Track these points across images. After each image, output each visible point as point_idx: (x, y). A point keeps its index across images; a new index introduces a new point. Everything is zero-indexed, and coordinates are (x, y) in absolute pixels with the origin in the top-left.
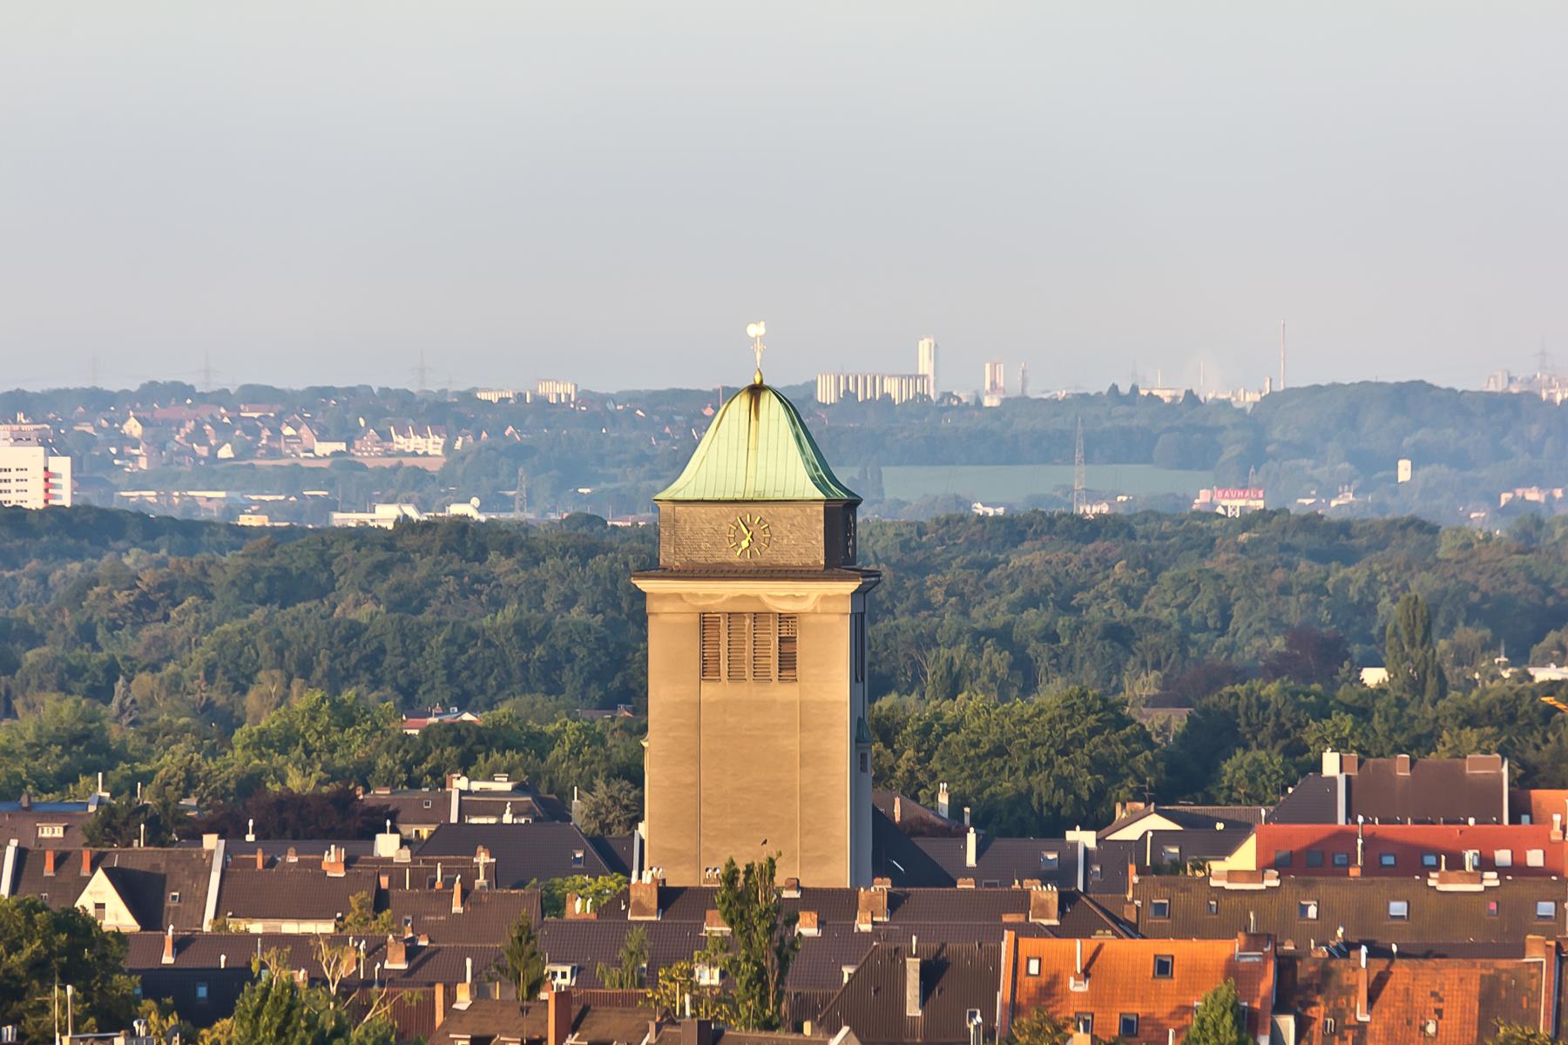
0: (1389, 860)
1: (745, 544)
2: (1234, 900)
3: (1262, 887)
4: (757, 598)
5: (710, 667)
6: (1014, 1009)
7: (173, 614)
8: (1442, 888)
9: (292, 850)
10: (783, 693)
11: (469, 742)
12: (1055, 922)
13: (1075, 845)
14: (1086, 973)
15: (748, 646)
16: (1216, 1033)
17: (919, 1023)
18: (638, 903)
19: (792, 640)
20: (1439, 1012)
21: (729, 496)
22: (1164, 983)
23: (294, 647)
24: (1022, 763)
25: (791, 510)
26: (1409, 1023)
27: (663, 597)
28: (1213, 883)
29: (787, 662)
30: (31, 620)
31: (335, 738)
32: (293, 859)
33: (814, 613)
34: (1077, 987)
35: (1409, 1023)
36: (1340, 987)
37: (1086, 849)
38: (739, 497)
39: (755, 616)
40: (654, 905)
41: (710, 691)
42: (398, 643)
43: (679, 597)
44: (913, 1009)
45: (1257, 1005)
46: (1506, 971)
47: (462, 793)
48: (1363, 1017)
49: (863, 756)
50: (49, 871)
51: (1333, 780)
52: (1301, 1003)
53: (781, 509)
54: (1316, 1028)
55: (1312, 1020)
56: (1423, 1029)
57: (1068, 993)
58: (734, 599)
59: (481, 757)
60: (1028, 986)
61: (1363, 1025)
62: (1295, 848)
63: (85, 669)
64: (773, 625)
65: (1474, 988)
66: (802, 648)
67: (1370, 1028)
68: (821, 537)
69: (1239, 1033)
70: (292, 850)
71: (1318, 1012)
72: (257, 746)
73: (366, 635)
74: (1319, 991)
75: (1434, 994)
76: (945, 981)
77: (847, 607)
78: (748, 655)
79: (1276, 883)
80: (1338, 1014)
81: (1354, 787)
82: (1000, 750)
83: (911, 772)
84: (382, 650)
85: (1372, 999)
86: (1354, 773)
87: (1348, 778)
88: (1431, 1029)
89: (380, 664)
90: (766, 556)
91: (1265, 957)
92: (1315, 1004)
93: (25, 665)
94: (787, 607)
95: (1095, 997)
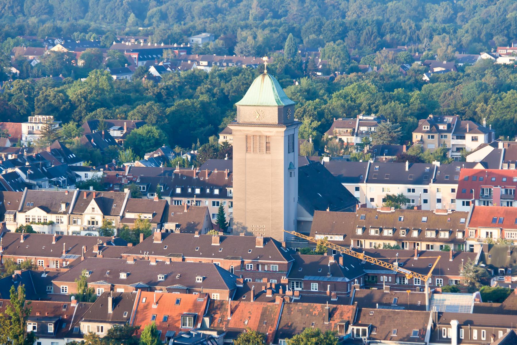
0: (494, 179)
1: (257, 117)
2: (382, 215)
3: (390, 212)
4: (260, 132)
5: (248, 149)
6: (137, 312)
7: (497, 3)
8: (436, 214)
9: (216, 169)
10: (267, 157)
11: (387, 98)
12: (262, 247)
13: (434, 165)
14: (157, 303)
15: (258, 144)
16: (146, 337)
17: (111, 315)
18: (156, 238)
19: (269, 143)
20: (250, 317)
21: (253, 104)
22: (178, 306)
23: (477, 29)
24: (513, 110)
25: (269, 108)
26: (241, 320)
27: (236, 131)
28: (378, 210)
29: (268, 148)
30: (462, 4)
31: (359, 95)
32: (216, 172)
33: (275, 136)
34: (154, 306)
35: (241, 320)
36: (225, 309)
37: (437, 167)
38: (256, 104)
39: (260, 136)
40: (160, 238)
41: (249, 156)
42: (514, 23)
43: (240, 131)
44: (110, 311)
45: (199, 314)
46: (270, 306)
47: (360, 120)
48: (229, 318)
49: (291, 173)
50: (85, 198)
51: (501, 150)
52: (214, 313)
53: (267, 108)
54: (216, 321)
55: (216, 318)
56: (244, 322)
57: (151, 308)
58: (254, 132)
59: (389, 103)
60: (141, 305)
61: (228, 321)
62: (470, 175)
63: (437, 29)
64: (264, 138)
65: (260, 311)
66: (272, 145)
67: (230, 322)
68: (277, 116)
69: (152, 337)
70: (216, 169)
71: (218, 316)
72: (338, 97)
73: (507, 21)
74: (219, 310)
75: (249, 312)
76: (121, 303)
77: (283, 135)
78: (258, 146)
79: (394, 211)
80: (223, 317)
81: (506, 152)
82: (509, 107)
83: (490, 111)
84: (510, 25)
85: (232, 313)
86: (507, 148)
87: (505, 150)
88: (246, 323)
89: (510, 28)
90: (263, 121)
91: (204, 300)
92: (217, 313)
93: (423, 28)
94: (268, 134)
95: (158, 310)
